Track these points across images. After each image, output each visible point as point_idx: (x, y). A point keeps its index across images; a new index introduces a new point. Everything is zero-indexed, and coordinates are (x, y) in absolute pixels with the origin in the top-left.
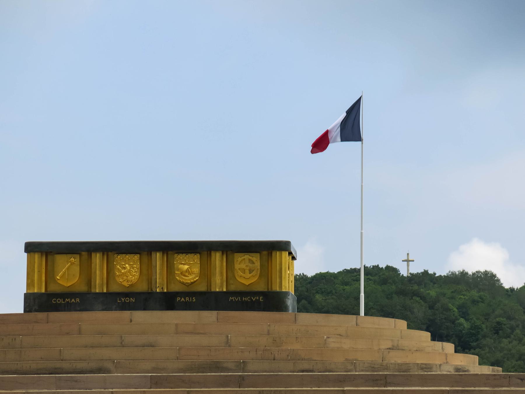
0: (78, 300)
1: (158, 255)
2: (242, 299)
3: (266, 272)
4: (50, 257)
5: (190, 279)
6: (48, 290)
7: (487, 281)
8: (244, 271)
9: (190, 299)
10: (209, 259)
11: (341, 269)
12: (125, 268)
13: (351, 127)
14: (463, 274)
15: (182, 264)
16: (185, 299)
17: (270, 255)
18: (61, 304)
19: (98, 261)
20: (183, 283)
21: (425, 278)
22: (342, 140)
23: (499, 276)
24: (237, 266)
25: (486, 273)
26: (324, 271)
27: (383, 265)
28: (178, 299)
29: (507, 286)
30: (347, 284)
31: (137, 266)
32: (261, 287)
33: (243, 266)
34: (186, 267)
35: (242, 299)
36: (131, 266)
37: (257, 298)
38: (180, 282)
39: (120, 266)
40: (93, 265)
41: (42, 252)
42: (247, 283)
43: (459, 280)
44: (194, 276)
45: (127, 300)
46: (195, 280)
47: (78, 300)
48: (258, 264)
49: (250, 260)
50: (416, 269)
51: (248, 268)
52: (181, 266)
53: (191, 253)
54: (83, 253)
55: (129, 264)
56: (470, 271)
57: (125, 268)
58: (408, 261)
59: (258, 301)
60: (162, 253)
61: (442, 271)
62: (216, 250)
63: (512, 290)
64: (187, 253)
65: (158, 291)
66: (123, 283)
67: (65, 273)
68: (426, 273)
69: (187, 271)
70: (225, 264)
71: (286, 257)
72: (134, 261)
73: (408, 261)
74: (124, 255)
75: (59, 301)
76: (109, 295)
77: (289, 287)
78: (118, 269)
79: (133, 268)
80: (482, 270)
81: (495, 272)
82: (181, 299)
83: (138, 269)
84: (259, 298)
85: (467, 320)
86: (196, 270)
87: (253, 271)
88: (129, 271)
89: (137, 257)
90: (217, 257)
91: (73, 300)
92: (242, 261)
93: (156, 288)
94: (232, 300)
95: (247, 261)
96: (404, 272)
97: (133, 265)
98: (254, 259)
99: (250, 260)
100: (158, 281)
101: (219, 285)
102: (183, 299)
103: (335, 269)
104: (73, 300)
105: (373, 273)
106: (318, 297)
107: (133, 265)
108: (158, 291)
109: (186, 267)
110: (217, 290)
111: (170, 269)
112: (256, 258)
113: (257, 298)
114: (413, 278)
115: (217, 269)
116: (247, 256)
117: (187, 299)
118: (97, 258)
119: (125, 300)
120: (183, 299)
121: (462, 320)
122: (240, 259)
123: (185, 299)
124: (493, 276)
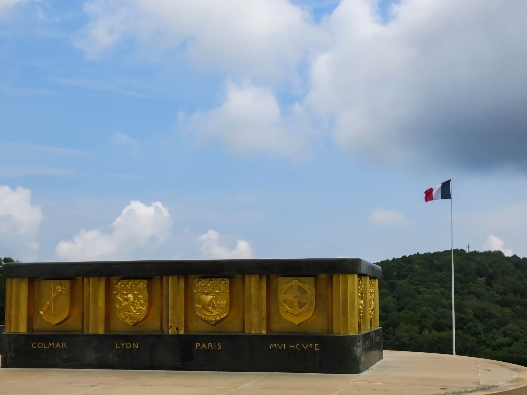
0: (64, 344)
2: (287, 346)
3: (324, 302)
4: (156, 283)
5: (214, 315)
6: (35, 327)
7: (499, 254)
8: (291, 305)
9: (213, 346)
11: (443, 250)
12: (126, 300)
13: (446, 191)
14: (490, 252)
16: (207, 346)
19: (91, 290)
20: (208, 322)
21: (475, 253)
22: (442, 198)
23: (503, 252)
24: (281, 297)
25: (498, 251)
26: (437, 251)
27: (459, 249)
28: (198, 345)
29: (506, 255)
30: (446, 256)
31: (143, 297)
32: (319, 327)
34: (210, 298)
35: (287, 346)
36: (136, 298)
38: (202, 319)
39: (121, 297)
40: (86, 295)
42: (297, 321)
43: (488, 254)
45: (128, 345)
46: (222, 316)
47: (64, 344)
48: (311, 292)
49: (299, 287)
50: (472, 250)
53: (217, 278)
55: (134, 295)
56: (492, 250)
58: (469, 247)
61: (481, 250)
62: (251, 273)
63: (508, 257)
64: (211, 277)
65: (170, 333)
66: (125, 321)
67: (50, 306)
68: (475, 251)
69: (211, 303)
70: (264, 293)
71: (353, 283)
72: (139, 290)
73: (469, 247)
74: (138, 281)
76: (110, 338)
79: (138, 299)
80: (497, 250)
81: (499, 250)
83: (145, 301)
84: (313, 346)
85: (491, 269)
86: (224, 302)
87: (305, 304)
88: (133, 304)
90: (255, 286)
91: (58, 345)
92: (288, 288)
93: (168, 328)
94: (273, 348)
96: (467, 251)
97: (138, 295)
98: (306, 286)
99: (299, 287)
100: (170, 318)
101: (256, 327)
102: (204, 346)
103: (441, 250)
104: (58, 345)
105: (456, 251)
106: (435, 261)
107: (138, 295)
108: (170, 333)
109: (210, 298)
110: (253, 332)
111: (189, 299)
114: (471, 254)
115: (253, 301)
116: (295, 282)
117: (210, 345)
118: (173, 286)
119: (125, 346)
120: (204, 346)
121: (490, 269)
122: (286, 286)
123: (207, 346)
124: (501, 252)
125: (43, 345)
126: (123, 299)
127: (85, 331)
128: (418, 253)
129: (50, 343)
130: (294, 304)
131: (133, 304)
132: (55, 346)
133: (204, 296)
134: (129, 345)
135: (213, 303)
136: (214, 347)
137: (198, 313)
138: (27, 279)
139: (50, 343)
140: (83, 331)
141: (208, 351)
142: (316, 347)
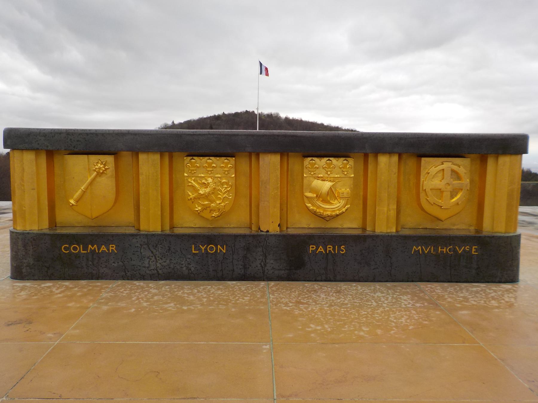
1: (383, 159)
2: (436, 250)
4: (57, 159)
5: (335, 206)
9: (334, 249)
10: (371, 167)
12: (206, 185)
15: (318, 178)
17: (483, 160)
18: (78, 256)
28: (312, 248)
33: (437, 183)
35: (436, 250)
37: (467, 248)
38: (315, 213)
41: (36, 150)
44: (343, 202)
47: (113, 248)
51: (449, 188)
52: (317, 183)
54: (243, 271)
55: (213, 178)
57: (206, 185)
59: (468, 256)
60: (395, 158)
69: (331, 192)
75: (75, 249)
77: (287, 185)
78: (193, 186)
82: (317, 249)
86: (345, 190)
89: (228, 163)
91: (103, 248)
92: (436, 173)
95: (448, 174)
98: (462, 171)
99: (453, 171)
102: (321, 249)
111: (291, 185)
112: (462, 166)
113: (467, 248)
117: (330, 248)
118: (149, 164)
119: (206, 249)
120: (321, 249)
122: (433, 170)
125: (80, 249)
126: (198, 183)
127: (369, 229)
128: (173, 122)
129: (90, 246)
130: (445, 194)
131: (211, 190)
132: (99, 250)
133: (320, 182)
134: (212, 249)
135: (328, 191)
136: (335, 251)
137: (309, 205)
138: (363, 154)
139: (90, 246)
140: (364, 229)
141: (326, 256)
142: (473, 250)
